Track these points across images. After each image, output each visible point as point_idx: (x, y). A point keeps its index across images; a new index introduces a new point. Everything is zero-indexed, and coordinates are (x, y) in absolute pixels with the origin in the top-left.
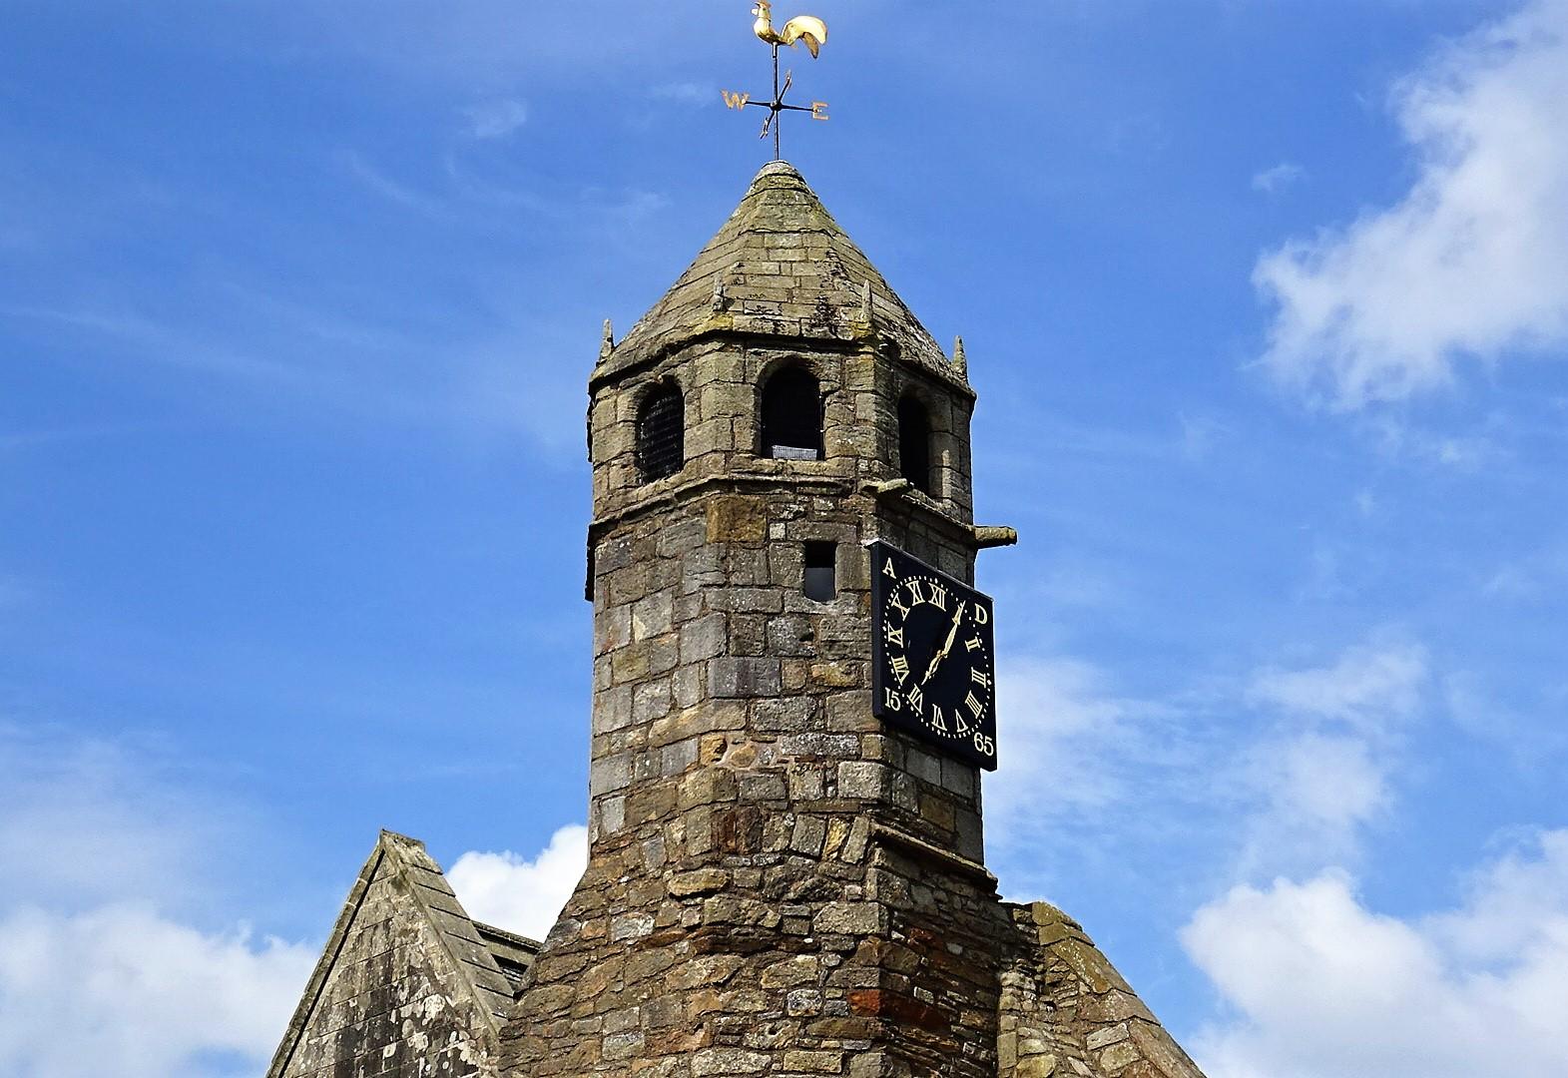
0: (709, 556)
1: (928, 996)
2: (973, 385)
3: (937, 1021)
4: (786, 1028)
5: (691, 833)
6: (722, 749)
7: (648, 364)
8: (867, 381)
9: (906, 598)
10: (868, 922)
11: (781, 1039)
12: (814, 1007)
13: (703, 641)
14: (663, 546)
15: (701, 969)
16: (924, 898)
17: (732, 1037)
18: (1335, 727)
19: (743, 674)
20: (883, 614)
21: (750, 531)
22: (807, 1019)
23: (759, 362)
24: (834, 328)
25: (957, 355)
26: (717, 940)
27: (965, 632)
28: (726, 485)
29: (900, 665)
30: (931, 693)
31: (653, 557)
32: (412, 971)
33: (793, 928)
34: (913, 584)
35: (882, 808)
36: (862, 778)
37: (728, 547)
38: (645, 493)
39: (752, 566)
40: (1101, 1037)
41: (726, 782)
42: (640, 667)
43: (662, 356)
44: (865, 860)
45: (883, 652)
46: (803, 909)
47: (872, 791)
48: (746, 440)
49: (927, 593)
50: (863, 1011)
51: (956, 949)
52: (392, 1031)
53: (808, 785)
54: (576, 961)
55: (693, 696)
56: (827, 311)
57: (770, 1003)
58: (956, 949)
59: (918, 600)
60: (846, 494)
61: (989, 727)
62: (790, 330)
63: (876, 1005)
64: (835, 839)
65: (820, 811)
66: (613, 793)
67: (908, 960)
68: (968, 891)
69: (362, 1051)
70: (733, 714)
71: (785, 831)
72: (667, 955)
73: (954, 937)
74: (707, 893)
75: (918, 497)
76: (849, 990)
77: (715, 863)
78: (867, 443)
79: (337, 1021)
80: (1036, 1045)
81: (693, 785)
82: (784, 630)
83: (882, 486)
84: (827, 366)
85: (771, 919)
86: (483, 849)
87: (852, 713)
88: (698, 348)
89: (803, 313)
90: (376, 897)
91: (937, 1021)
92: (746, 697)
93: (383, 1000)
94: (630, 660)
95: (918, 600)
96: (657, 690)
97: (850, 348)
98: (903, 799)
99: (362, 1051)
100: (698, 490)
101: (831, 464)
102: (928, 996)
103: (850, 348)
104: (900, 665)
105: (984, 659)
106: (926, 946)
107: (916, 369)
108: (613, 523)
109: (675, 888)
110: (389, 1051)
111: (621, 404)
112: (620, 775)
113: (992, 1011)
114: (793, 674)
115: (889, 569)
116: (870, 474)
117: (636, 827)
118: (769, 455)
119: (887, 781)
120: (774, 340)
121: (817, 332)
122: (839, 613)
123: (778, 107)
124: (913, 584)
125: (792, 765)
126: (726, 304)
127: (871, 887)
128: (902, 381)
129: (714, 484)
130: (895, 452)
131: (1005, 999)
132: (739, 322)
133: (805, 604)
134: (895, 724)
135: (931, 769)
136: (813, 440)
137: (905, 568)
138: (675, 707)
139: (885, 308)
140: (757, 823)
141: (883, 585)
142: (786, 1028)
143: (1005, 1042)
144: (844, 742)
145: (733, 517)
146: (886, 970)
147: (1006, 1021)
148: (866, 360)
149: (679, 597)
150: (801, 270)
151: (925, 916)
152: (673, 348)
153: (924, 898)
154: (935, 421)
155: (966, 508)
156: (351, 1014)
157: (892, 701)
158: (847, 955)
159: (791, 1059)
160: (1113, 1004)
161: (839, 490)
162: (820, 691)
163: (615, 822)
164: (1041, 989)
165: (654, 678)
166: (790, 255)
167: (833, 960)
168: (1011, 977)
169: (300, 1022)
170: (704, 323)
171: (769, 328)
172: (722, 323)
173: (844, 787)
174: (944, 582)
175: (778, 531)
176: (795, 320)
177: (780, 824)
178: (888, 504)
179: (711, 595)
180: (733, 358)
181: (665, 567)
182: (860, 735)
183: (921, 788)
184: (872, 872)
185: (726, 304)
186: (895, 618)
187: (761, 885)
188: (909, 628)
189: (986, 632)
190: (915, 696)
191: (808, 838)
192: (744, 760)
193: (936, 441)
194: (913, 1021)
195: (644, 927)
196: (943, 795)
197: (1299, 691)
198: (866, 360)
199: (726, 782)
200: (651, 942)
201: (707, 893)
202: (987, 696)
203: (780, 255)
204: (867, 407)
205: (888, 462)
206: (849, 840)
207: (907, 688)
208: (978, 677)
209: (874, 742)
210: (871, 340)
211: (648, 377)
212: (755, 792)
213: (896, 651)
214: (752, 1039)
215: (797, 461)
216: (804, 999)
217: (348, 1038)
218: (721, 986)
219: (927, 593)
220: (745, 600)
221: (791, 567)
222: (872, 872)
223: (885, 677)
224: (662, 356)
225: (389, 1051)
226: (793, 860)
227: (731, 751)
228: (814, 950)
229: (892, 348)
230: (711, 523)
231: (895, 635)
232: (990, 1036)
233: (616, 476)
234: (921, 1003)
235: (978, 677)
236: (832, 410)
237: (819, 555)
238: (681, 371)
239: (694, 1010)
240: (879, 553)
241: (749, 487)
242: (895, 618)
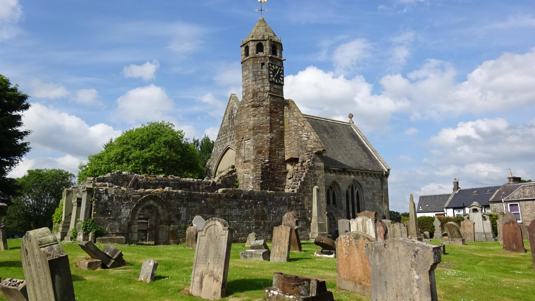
0: (251, 65)
1: (275, 110)
2: (282, 42)
3: (276, 113)
4: (260, 115)
5: (250, 95)
6: (253, 86)
7: (245, 44)
8: (268, 44)
9: (272, 68)
10: (268, 103)
11: (260, 116)
12: (263, 112)
13: (251, 75)
14: (248, 65)
15: (252, 109)
16: (275, 100)
17: (255, 116)
18: (401, 44)
19: (255, 78)
20: (270, 70)
21: (255, 62)
22: (262, 114)
23: (256, 43)
24: (264, 38)
25: (280, 39)
26: (253, 106)
27: (280, 70)
28: (253, 57)
29: (272, 76)
30: (275, 78)
31: (247, 66)
32: (234, 108)
33: (260, 105)
34: (273, 66)
35: (270, 91)
36: (268, 88)
37: (253, 64)
38: (246, 59)
39: (256, 66)
40: (295, 113)
41: (254, 90)
42: (246, 78)
43: (247, 43)
44: (268, 97)
45: (270, 74)
46: (262, 103)
47: (269, 90)
48: (255, 52)
49: (275, 67)
50: (268, 113)
51: (279, 105)
52: (233, 115)
53: (262, 90)
54: (241, 109)
55: (250, 81)
56: (264, 36)
57: (258, 113)
58: (279, 105)
59: (274, 68)
60: (266, 57)
61: (283, 81)
62: (259, 39)
63: (269, 112)
64: (265, 95)
65: (263, 92)
66: (244, 91)
67: (273, 107)
68: (280, 99)
69: (230, 117)
70: (254, 82)
71: (260, 94)
72: (249, 108)
73: (279, 104)
74: (252, 102)
75: (274, 56)
76: (266, 111)
77: (253, 98)
78: (268, 51)
79: (228, 114)
80: (287, 114)
81: (251, 90)
82: (259, 73)
83: (269, 56)
84: (263, 43)
85: (258, 104)
86: (288, 75)
87: (266, 81)
88: (250, 42)
89: (261, 37)
90: (231, 101)
91: (276, 113)
92: (256, 81)
93: (232, 111)
94: (245, 77)
95: (274, 68)
96: (247, 80)
97: (266, 40)
98: (272, 90)
99: (230, 117)
100: (250, 58)
101: (264, 54)
102: (275, 110)
103: (266, 40)
104: (272, 76)
105: (283, 74)
106: (275, 105)
107: (274, 42)
108: (243, 62)
109: (249, 101)
110: (233, 117)
111: (243, 48)
112: (244, 90)
113: (283, 111)
114: (260, 78)
115: (270, 65)
116: (268, 55)
117: (246, 95)
118: (258, 53)
119: (270, 88)
120: (257, 40)
121: (262, 39)
122: (265, 70)
123: (261, 10)
124: (273, 66)
125: (260, 88)
126: (253, 37)
127: (269, 100)
128: (272, 43)
129: (251, 57)
130: (271, 52)
131: (285, 110)
132: (254, 39)
133: (261, 70)
134: (270, 82)
135: (276, 86)
136: (263, 51)
137: (272, 65)
138: (249, 82)
139: (271, 34)
140: (257, 93)
141: (269, 67)
142: (260, 115)
143: (285, 114)
144: (266, 85)
145: (254, 61)
146: (270, 108)
147: (285, 112)
148: (268, 42)
149: (249, 70)
150: (262, 31)
151: (275, 102)
152: (248, 42)
153: (275, 100)
154: (277, 47)
155: (281, 57)
156: (229, 113)
157: (271, 80)
158: (266, 107)
159: (261, 118)
160: (296, 110)
161: (265, 57)
162: (263, 79)
163: (244, 94)
164: (289, 108)
165: (247, 79)
166: (261, 29)
167: (265, 108)
168: (285, 107)
169: (225, 114)
170: (250, 39)
171: (257, 39)
172: (252, 39)
173: (266, 89)
174: (277, 66)
175: (258, 62)
176: (260, 38)
177: (259, 94)
178: (270, 58)
179: (252, 70)
180: (253, 43)
181: (248, 67)
182: (267, 84)
183: (275, 88)
184: (269, 98)
185: (253, 37)
186: (271, 71)
187: (257, 100)
188: (273, 72)
189: (283, 71)
190: (274, 79)
191: (262, 95)
192: (255, 87)
193: (277, 49)
194: (274, 113)
195: (247, 105)
196: (277, 89)
197: (397, 39)
198: (268, 42)
199: (254, 90)
200: (248, 107)
201: (252, 102)
202: (283, 78)
203: (260, 29)
204: (268, 47)
205: (270, 53)
206: (266, 95)
207: (273, 78)
208: (281, 75)
209: (269, 84)
210: (268, 39)
211: (246, 45)
212: (257, 90)
213: (271, 74)
214: (257, 116)
215: (261, 54)
216: (262, 112)
217: (229, 115)
218: (254, 111)
219: (275, 67)
220: (255, 70)
221: (260, 66)
222: (269, 98)
223: (270, 77)
224: (247, 43)
225: (233, 117)
226: (261, 98)
227: (254, 86)
228: (263, 107)
229: (271, 39)
230: (251, 62)
231: (271, 72)
232: (283, 114)
233: (243, 57)
234: (275, 111)
235: (281, 75)
236: (264, 48)
237: (263, 64)
238: (248, 45)
239: (251, 114)
240: (269, 64)
241: (255, 57)
242: (271, 71)
